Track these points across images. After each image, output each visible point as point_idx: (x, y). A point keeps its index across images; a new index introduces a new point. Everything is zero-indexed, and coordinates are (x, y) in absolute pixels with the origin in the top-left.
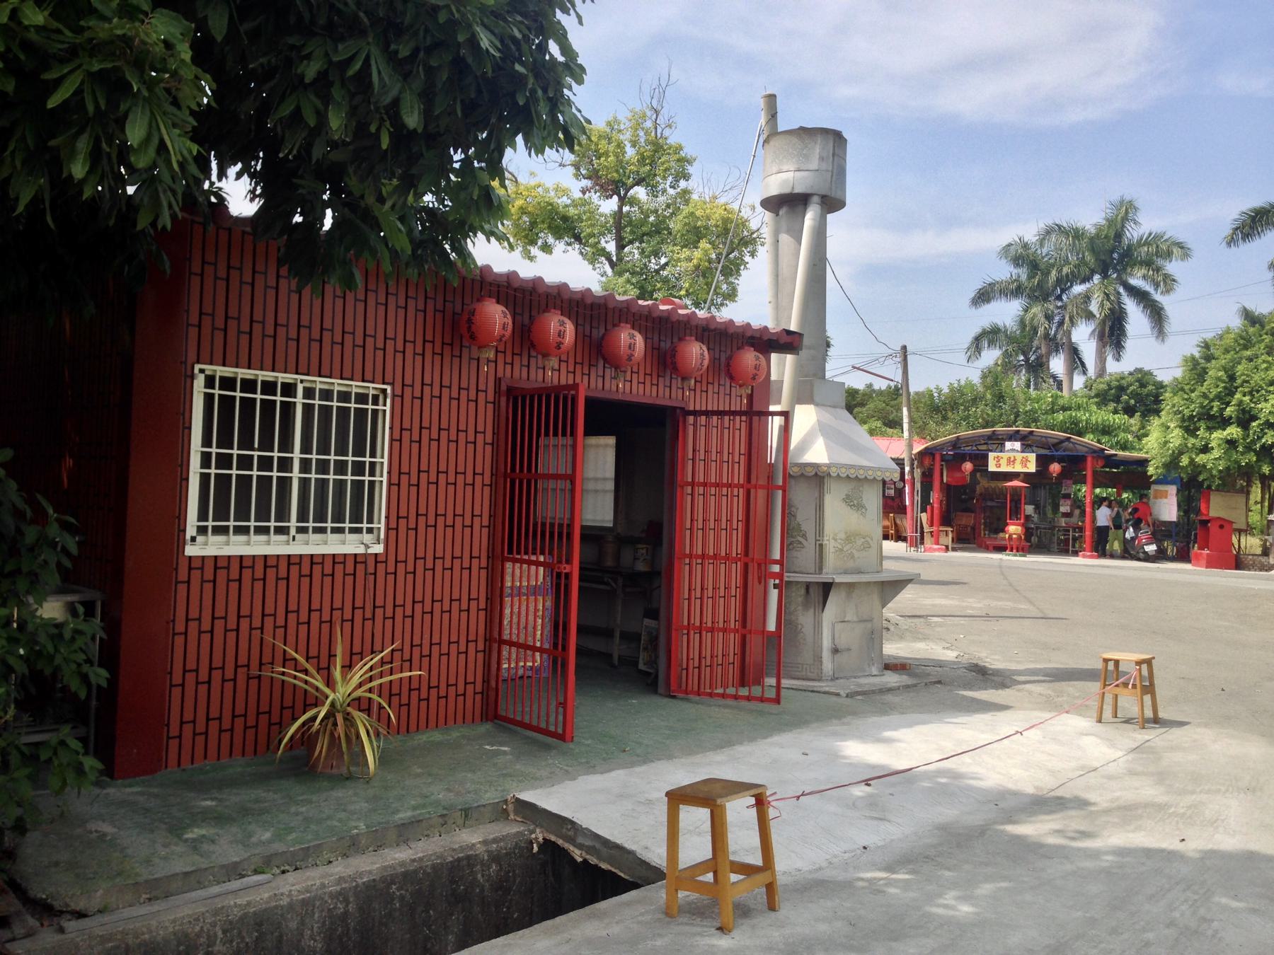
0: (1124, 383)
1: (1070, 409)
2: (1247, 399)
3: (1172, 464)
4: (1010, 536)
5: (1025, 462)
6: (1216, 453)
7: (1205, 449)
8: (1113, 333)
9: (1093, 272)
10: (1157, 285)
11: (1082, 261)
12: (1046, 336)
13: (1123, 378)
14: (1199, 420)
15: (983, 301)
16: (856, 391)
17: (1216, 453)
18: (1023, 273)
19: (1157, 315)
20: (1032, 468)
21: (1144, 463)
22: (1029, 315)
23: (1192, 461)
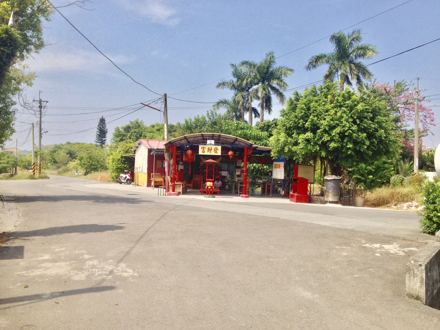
0: (270, 124)
1: (244, 129)
2: (316, 118)
3: (281, 151)
4: (208, 187)
5: (216, 150)
6: (301, 146)
7: (296, 144)
9: (259, 81)
14: (294, 129)
16: (173, 126)
17: (301, 146)
19: (281, 95)
20: (219, 153)
21: (269, 151)
23: (290, 150)
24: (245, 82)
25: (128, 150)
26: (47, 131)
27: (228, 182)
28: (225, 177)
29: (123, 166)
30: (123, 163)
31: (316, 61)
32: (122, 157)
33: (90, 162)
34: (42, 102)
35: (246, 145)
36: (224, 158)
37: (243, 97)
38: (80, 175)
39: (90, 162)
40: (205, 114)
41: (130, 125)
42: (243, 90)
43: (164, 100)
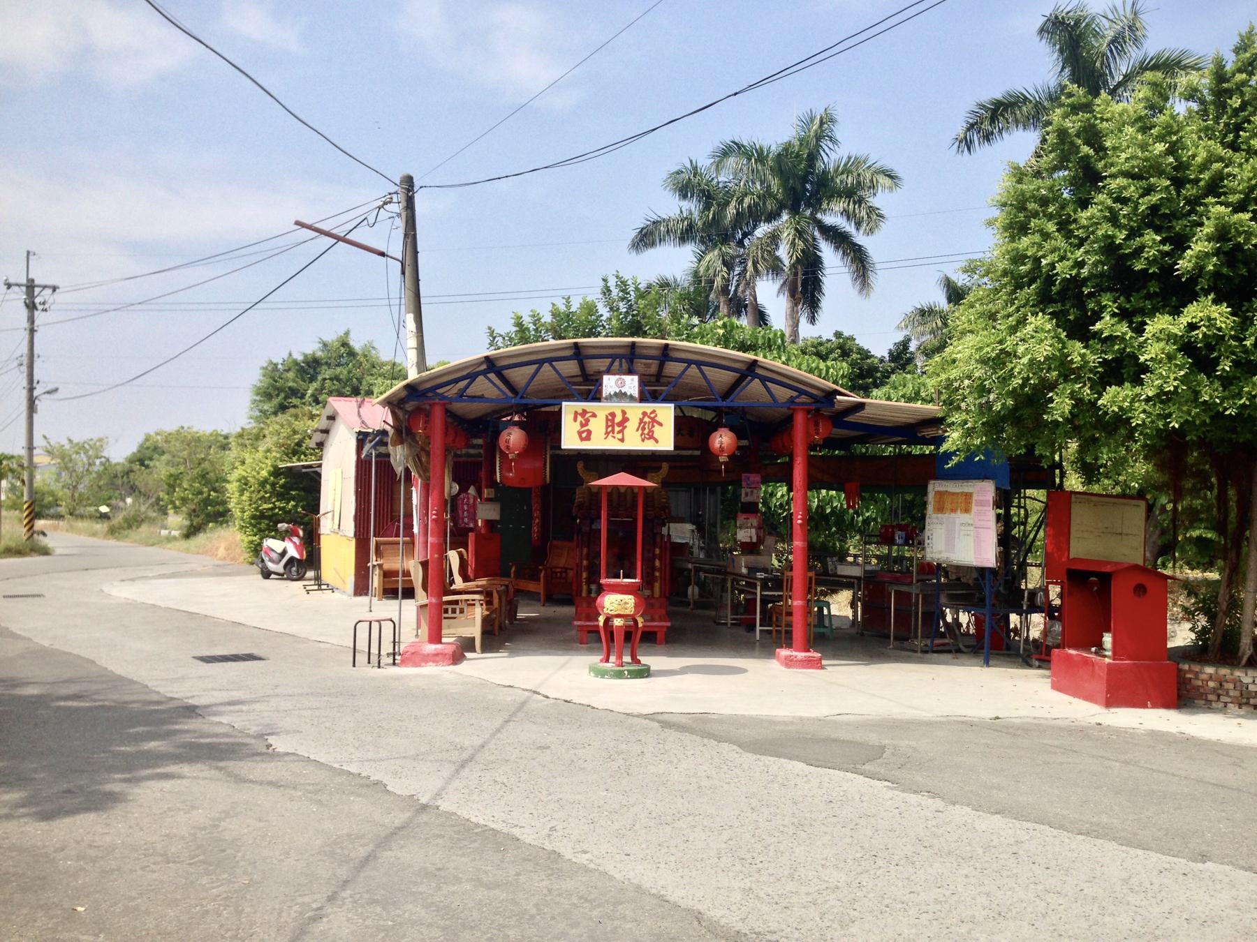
4: (608, 620)
5: (648, 426)
7: (1124, 368)
8: (806, 288)
9: (782, 206)
10: (858, 225)
11: (768, 193)
12: (725, 290)
13: (821, 344)
15: (646, 245)
18: (691, 207)
20: (665, 440)
22: (704, 263)
24: (731, 211)
25: (299, 444)
26: (56, 390)
27: (697, 570)
28: (681, 549)
29: (280, 509)
30: (282, 496)
31: (996, 116)
32: (276, 472)
33: (201, 493)
34: (37, 290)
35: (804, 399)
36: (686, 468)
37: (725, 263)
38: (175, 538)
39: (201, 493)
40: (595, 295)
41: (319, 354)
42: (725, 238)
43: (403, 204)
